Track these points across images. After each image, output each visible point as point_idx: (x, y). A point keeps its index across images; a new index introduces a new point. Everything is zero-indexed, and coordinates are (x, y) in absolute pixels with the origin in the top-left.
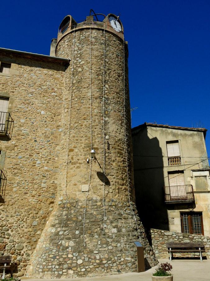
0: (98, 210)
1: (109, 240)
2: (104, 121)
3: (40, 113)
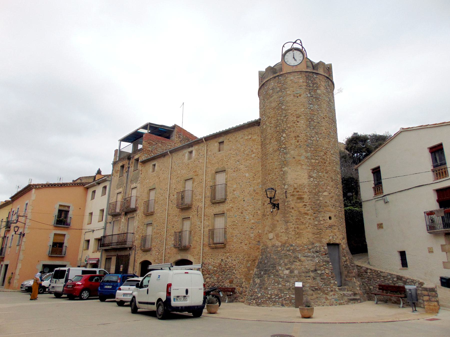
0: (277, 255)
2: (282, 172)
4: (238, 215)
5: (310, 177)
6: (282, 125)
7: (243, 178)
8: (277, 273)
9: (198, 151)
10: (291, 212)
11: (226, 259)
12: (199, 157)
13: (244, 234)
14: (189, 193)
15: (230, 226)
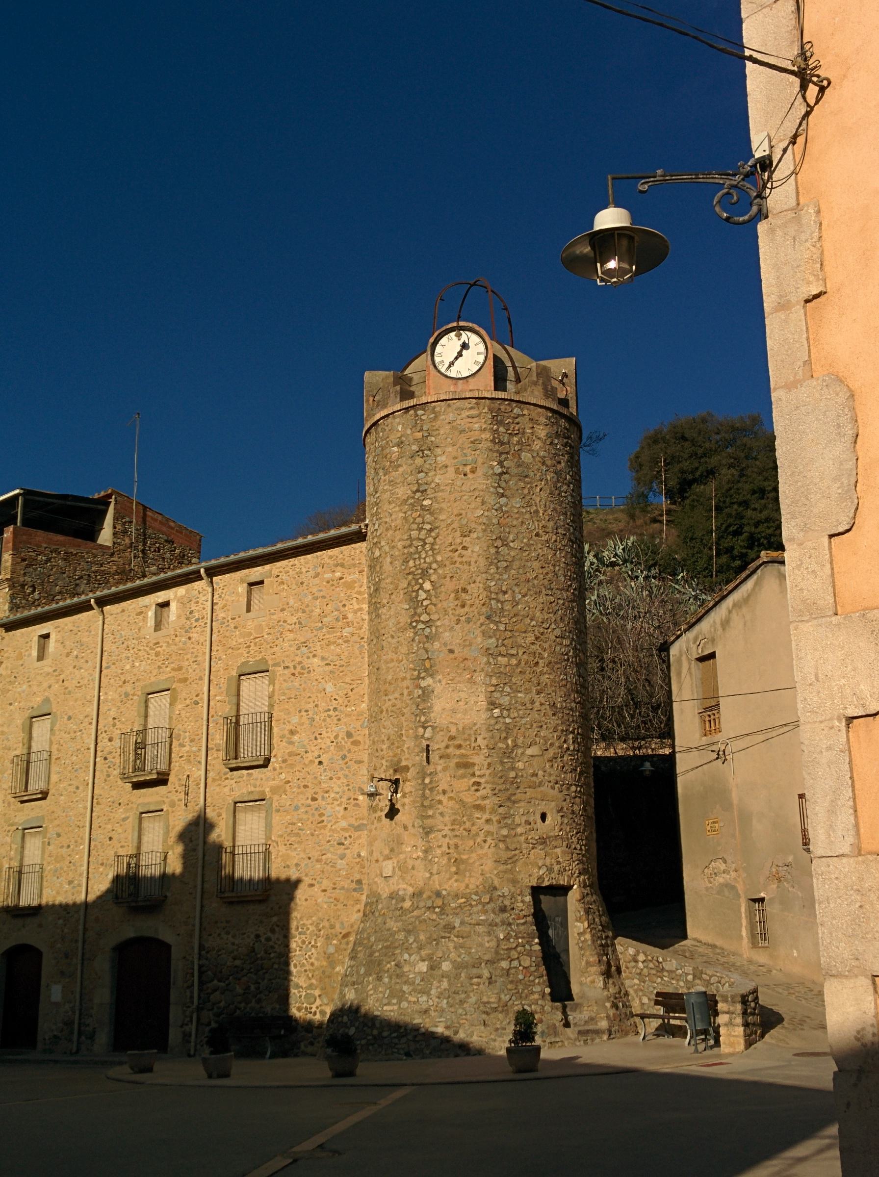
1: (405, 988)
3: (324, 690)
4: (303, 804)
5: (493, 704)
6: (423, 556)
7: (319, 695)
8: (398, 969)
9: (188, 605)
10: (440, 802)
11: (269, 934)
12: (188, 622)
13: (318, 861)
14: (160, 735)
15: (281, 836)
